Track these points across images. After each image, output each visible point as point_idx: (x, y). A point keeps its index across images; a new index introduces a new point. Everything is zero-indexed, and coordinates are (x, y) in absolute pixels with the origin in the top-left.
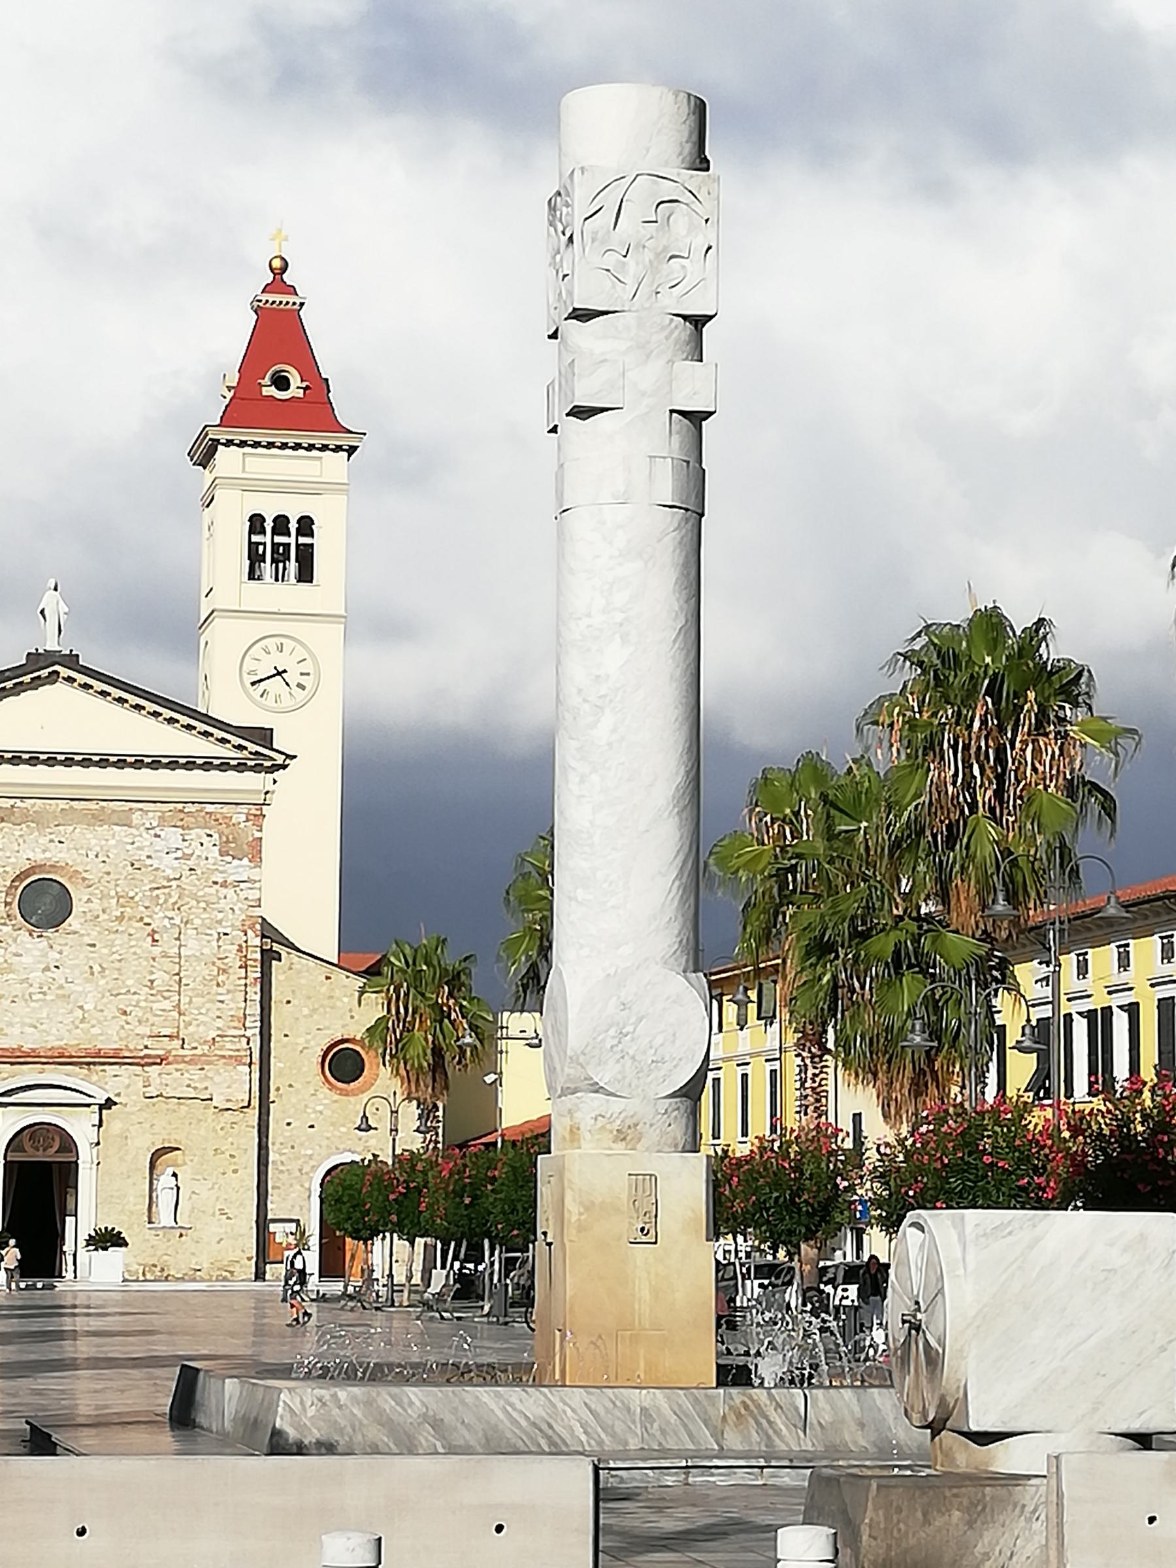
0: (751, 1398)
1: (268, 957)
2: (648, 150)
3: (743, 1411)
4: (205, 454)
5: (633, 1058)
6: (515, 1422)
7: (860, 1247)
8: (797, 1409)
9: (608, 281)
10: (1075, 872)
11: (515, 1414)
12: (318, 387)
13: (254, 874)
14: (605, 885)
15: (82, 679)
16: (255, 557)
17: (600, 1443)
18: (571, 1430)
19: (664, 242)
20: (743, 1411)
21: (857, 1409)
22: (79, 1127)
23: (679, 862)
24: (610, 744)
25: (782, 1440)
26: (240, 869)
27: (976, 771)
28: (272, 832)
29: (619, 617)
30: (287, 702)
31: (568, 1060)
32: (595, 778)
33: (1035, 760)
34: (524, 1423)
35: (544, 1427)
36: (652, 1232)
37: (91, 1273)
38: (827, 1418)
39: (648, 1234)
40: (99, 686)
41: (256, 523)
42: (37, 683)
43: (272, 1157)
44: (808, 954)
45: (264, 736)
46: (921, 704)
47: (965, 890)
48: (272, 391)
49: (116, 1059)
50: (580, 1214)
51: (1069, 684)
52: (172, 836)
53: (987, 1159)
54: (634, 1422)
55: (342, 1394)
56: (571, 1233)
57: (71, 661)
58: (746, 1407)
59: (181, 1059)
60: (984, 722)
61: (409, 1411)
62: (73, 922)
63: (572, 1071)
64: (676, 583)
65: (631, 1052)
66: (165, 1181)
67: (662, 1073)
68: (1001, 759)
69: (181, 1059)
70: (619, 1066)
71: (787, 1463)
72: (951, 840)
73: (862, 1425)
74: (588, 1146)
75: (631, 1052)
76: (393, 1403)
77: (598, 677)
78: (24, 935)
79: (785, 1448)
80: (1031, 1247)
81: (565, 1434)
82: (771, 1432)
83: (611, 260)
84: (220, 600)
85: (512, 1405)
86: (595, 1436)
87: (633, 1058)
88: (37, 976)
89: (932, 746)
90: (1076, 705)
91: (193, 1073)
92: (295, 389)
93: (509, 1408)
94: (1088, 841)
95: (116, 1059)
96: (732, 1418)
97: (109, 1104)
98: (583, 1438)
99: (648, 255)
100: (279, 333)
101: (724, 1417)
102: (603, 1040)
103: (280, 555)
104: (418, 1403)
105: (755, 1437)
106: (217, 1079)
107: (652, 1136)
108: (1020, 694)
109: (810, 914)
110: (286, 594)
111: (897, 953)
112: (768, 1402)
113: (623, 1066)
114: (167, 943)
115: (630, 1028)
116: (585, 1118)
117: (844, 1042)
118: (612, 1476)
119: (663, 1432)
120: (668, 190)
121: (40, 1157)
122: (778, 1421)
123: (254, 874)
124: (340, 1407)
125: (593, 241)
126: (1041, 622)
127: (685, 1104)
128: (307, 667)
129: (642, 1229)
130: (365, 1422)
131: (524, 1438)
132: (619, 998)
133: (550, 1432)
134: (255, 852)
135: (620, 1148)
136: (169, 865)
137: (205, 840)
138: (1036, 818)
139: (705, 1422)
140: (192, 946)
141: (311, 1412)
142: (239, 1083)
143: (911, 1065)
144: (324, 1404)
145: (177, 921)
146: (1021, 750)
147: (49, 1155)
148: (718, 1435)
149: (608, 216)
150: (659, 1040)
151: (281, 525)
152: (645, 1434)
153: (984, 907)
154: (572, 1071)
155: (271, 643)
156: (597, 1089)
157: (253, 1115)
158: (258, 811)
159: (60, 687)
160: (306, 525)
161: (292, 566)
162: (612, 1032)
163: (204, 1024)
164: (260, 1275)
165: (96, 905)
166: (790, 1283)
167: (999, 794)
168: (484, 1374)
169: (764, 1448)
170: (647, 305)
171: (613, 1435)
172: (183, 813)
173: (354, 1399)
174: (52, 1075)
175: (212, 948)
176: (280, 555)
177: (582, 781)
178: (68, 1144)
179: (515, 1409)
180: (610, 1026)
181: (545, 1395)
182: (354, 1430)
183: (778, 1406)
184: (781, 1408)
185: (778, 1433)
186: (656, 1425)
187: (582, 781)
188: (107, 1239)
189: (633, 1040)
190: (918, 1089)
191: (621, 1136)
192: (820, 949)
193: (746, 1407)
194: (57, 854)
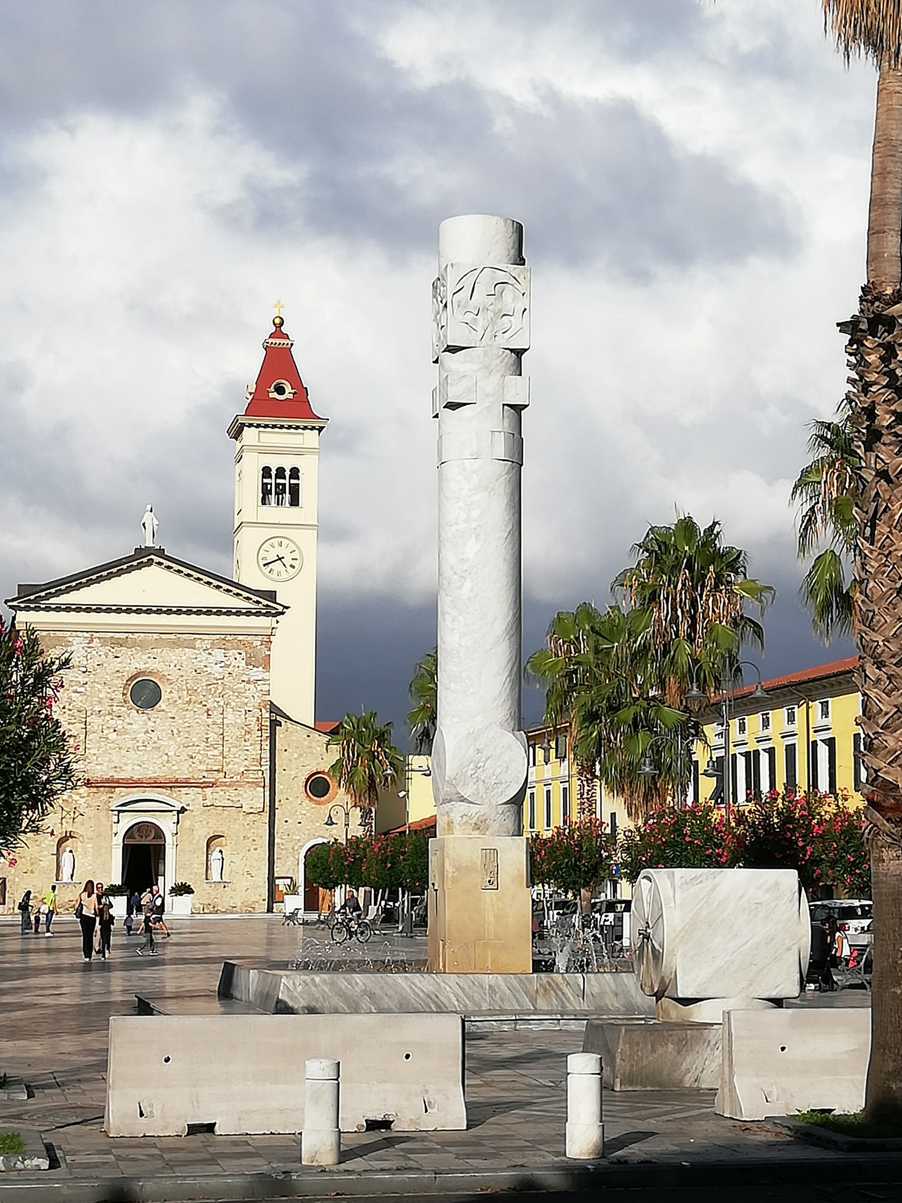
1: (274, 724)
4: (237, 432)
5: (484, 781)
7: (615, 891)
8: (579, 985)
10: (738, 669)
13: (266, 676)
16: (266, 492)
18: (449, 998)
19: (499, 307)
21: (613, 985)
22: (166, 824)
24: (469, 599)
25: (570, 1004)
26: (257, 673)
29: (474, 525)
30: (284, 576)
32: (461, 618)
33: (715, 607)
34: (422, 995)
35: (434, 997)
36: (495, 883)
38: (596, 991)
39: (493, 883)
41: (266, 472)
42: (140, 566)
45: (271, 595)
46: (648, 574)
48: (275, 395)
49: (187, 784)
52: (219, 654)
54: (485, 994)
56: (448, 884)
57: (160, 553)
58: (550, 985)
59: (224, 784)
60: (684, 585)
62: (162, 704)
66: (216, 855)
67: (501, 790)
69: (224, 784)
73: (616, 994)
74: (458, 833)
80: (713, 890)
83: (469, 317)
84: (245, 517)
87: (484, 781)
91: (231, 792)
94: (747, 651)
95: (187, 784)
96: (541, 991)
97: (183, 810)
98: (456, 1003)
100: (279, 361)
101: (537, 991)
102: (466, 771)
106: (245, 795)
107: (495, 826)
114: (216, 716)
116: (456, 816)
119: (502, 1000)
120: (501, 277)
123: (266, 676)
124: (316, 986)
127: (513, 808)
129: (489, 881)
133: (437, 1000)
134: (266, 663)
135: (476, 834)
137: (238, 656)
140: (230, 718)
141: (299, 989)
142: (257, 798)
145: (222, 703)
146: (706, 601)
147: (148, 841)
148: (534, 1001)
150: (498, 771)
151: (280, 472)
156: (463, 799)
157: (266, 817)
160: (295, 473)
161: (287, 496)
162: (471, 766)
164: (270, 910)
165: (175, 695)
167: (693, 627)
170: (489, 343)
172: (225, 640)
177: (453, 620)
180: (471, 763)
185: (568, 999)
187: (453, 620)
188: (182, 889)
190: (647, 798)
191: (477, 827)
193: (550, 985)
194: (153, 665)
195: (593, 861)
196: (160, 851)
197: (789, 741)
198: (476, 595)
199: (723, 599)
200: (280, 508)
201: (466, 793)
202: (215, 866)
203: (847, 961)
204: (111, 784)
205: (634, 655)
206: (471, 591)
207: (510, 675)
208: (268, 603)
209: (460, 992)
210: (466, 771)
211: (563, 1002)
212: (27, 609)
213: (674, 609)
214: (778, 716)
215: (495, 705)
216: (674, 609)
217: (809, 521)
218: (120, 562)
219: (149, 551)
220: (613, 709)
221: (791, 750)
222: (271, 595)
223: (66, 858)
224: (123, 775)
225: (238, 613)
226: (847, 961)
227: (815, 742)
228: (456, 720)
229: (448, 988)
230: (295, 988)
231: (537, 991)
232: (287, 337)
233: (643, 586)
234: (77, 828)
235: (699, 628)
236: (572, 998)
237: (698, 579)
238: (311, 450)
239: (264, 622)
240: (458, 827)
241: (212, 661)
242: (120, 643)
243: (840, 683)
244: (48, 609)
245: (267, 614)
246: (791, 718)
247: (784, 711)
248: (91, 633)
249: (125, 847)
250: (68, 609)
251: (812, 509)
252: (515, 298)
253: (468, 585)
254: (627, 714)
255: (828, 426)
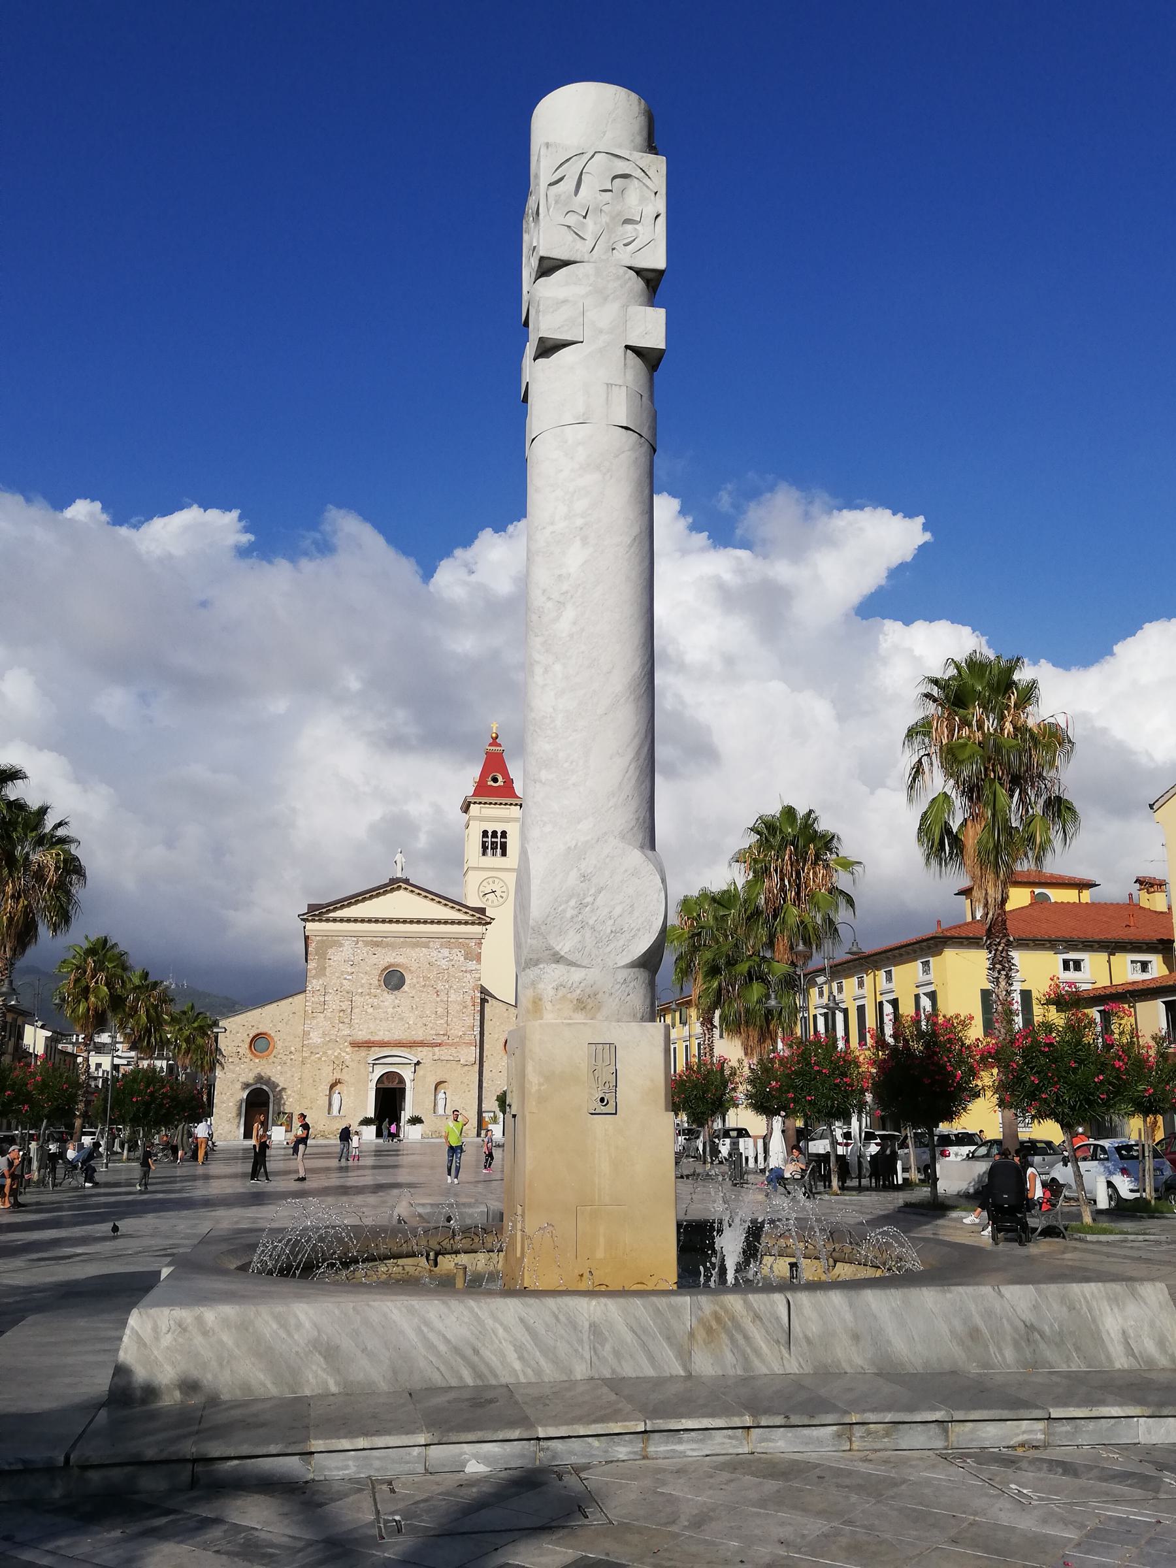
0: (723, 1307)
1: (483, 1001)
2: (604, 133)
3: (714, 1325)
4: (466, 808)
5: (593, 928)
6: (431, 1347)
7: (724, 1121)
8: (778, 1319)
9: (570, 236)
10: (836, 930)
11: (431, 1336)
12: (509, 782)
13: (478, 967)
14: (566, 765)
15: (411, 888)
16: (485, 848)
17: (538, 1372)
18: (502, 1355)
19: (619, 207)
20: (714, 1325)
21: (848, 1317)
22: (407, 1074)
23: (637, 742)
24: (571, 636)
25: (763, 1361)
26: (472, 965)
27: (786, 883)
28: (485, 950)
29: (579, 522)
30: (496, 903)
31: (530, 931)
32: (558, 667)
33: (814, 877)
34: (443, 1348)
35: (469, 1352)
36: (612, 1103)
37: (411, 1134)
38: (814, 1329)
39: (607, 1104)
40: (424, 894)
41: (485, 833)
42: (392, 890)
43: (484, 1085)
44: (706, 975)
45: (482, 911)
46: (759, 852)
47: (782, 944)
48: (491, 783)
49: (422, 1044)
50: (540, 1084)
51: (827, 842)
52: (445, 952)
53: (816, 1068)
54: (581, 1341)
55: (210, 1315)
56: (532, 1105)
57: (406, 881)
58: (718, 1319)
59: (447, 1044)
60: (790, 858)
61: (296, 1337)
62: (405, 988)
63: (534, 942)
64: (630, 546)
65: (591, 922)
66: (441, 1095)
67: (621, 943)
68: (798, 874)
69: (447, 1044)
70: (579, 936)
71: (779, 1420)
72: (775, 917)
73: (856, 1338)
74: (549, 1017)
75: (591, 922)
76: (275, 1326)
77: (560, 576)
78: (385, 994)
79: (765, 1371)
81: (494, 1361)
82: (749, 1350)
83: (572, 220)
84: (471, 864)
85: (427, 1323)
86: (533, 1363)
87: (593, 928)
88: (390, 1010)
89: (766, 871)
90: (831, 853)
91: (453, 1050)
92: (500, 783)
93: (425, 1329)
94: (842, 915)
95: (422, 1044)
96: (701, 1335)
97: (418, 1063)
98: (517, 1365)
99: (605, 219)
101: (692, 1335)
102: (564, 911)
103: (494, 846)
104: (307, 1325)
105: (729, 1358)
107: (611, 1005)
108: (806, 846)
109: (708, 955)
110: (496, 861)
111: (749, 972)
112: (745, 1313)
113: (583, 936)
114: (443, 997)
115: (589, 899)
116: (547, 989)
117: (723, 1018)
118: (541, 1450)
119: (617, 1354)
120: (621, 167)
121: (391, 1086)
122: (757, 1336)
123: (478, 967)
124: (205, 1333)
125: (556, 202)
126: (811, 811)
127: (642, 975)
128: (504, 889)
129: (602, 1100)
130: (237, 1352)
131: (442, 1368)
132: (579, 870)
133: (475, 1359)
134: (478, 958)
135: (579, 1018)
136: (444, 964)
138: (816, 905)
139: (668, 1339)
140: (453, 997)
141: (167, 1340)
142: (472, 1053)
143: (758, 1025)
144: (185, 1330)
146: (808, 872)
147: (394, 1085)
148: (685, 1356)
149: (568, 185)
150: (618, 910)
151: (494, 834)
152: (594, 1359)
153: (792, 948)
154: (534, 942)
155: (490, 880)
156: (558, 959)
157: (477, 1067)
158: (479, 941)
159: (402, 891)
160: (504, 834)
161: (499, 850)
162: (572, 903)
163: (457, 1030)
164: (479, 1135)
165: (415, 980)
166: (698, 1138)
167: (798, 894)
168: (472, 1235)
169: (740, 1372)
170: (604, 257)
171: (556, 1361)
172: (450, 942)
173: (225, 1322)
174: (395, 1052)
175: (462, 997)
176: (494, 846)
177: (546, 671)
178: (401, 1080)
179: (432, 1329)
180: (571, 897)
181: (471, 1310)
182: (221, 1365)
183: (757, 1317)
184: (761, 1319)
185: (757, 1352)
186: (608, 1347)
187: (546, 671)
188: (415, 1120)
189: (592, 911)
190: (762, 1041)
191: (581, 1005)
192: (713, 971)
193: (718, 1319)
194: (400, 960)
195: (719, 1093)
196: (402, 1091)
197: (860, 1002)
198: (583, 630)
199: (821, 872)
200: (494, 858)
201: (564, 946)
202: (441, 1103)
203: (1041, 1204)
204: (368, 1045)
205: (749, 918)
206: (574, 623)
207: (638, 753)
208: (480, 916)
209: (525, 1339)
210: (564, 911)
211: (746, 1359)
212: (313, 921)
213: (782, 880)
214: (850, 984)
215: (611, 804)
216: (782, 880)
217: (918, 770)
218: (379, 888)
219: (398, 880)
220: (731, 963)
221: (861, 1010)
222: (482, 911)
223: (336, 1098)
224: (377, 1038)
225: (460, 923)
226: (1041, 1204)
227: (881, 1003)
228: (548, 828)
229: (501, 1331)
230: (157, 1339)
231: (692, 1335)
232: (500, 745)
233: (755, 861)
234: (344, 1076)
235: (802, 895)
236: (765, 1348)
237: (801, 856)
238: (516, 820)
239: (478, 929)
240: (549, 1006)
241: (442, 956)
242: (377, 944)
243: (901, 955)
244: (328, 920)
245: (479, 924)
246: (861, 984)
247: (855, 980)
248: (357, 936)
249: (378, 1090)
250: (342, 920)
251: (920, 761)
252: (643, 199)
253: (569, 613)
254: (743, 968)
255: (936, 682)
